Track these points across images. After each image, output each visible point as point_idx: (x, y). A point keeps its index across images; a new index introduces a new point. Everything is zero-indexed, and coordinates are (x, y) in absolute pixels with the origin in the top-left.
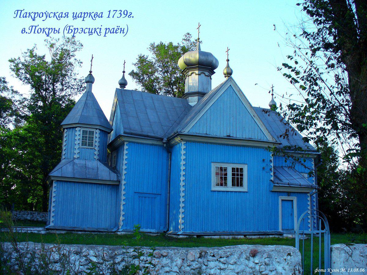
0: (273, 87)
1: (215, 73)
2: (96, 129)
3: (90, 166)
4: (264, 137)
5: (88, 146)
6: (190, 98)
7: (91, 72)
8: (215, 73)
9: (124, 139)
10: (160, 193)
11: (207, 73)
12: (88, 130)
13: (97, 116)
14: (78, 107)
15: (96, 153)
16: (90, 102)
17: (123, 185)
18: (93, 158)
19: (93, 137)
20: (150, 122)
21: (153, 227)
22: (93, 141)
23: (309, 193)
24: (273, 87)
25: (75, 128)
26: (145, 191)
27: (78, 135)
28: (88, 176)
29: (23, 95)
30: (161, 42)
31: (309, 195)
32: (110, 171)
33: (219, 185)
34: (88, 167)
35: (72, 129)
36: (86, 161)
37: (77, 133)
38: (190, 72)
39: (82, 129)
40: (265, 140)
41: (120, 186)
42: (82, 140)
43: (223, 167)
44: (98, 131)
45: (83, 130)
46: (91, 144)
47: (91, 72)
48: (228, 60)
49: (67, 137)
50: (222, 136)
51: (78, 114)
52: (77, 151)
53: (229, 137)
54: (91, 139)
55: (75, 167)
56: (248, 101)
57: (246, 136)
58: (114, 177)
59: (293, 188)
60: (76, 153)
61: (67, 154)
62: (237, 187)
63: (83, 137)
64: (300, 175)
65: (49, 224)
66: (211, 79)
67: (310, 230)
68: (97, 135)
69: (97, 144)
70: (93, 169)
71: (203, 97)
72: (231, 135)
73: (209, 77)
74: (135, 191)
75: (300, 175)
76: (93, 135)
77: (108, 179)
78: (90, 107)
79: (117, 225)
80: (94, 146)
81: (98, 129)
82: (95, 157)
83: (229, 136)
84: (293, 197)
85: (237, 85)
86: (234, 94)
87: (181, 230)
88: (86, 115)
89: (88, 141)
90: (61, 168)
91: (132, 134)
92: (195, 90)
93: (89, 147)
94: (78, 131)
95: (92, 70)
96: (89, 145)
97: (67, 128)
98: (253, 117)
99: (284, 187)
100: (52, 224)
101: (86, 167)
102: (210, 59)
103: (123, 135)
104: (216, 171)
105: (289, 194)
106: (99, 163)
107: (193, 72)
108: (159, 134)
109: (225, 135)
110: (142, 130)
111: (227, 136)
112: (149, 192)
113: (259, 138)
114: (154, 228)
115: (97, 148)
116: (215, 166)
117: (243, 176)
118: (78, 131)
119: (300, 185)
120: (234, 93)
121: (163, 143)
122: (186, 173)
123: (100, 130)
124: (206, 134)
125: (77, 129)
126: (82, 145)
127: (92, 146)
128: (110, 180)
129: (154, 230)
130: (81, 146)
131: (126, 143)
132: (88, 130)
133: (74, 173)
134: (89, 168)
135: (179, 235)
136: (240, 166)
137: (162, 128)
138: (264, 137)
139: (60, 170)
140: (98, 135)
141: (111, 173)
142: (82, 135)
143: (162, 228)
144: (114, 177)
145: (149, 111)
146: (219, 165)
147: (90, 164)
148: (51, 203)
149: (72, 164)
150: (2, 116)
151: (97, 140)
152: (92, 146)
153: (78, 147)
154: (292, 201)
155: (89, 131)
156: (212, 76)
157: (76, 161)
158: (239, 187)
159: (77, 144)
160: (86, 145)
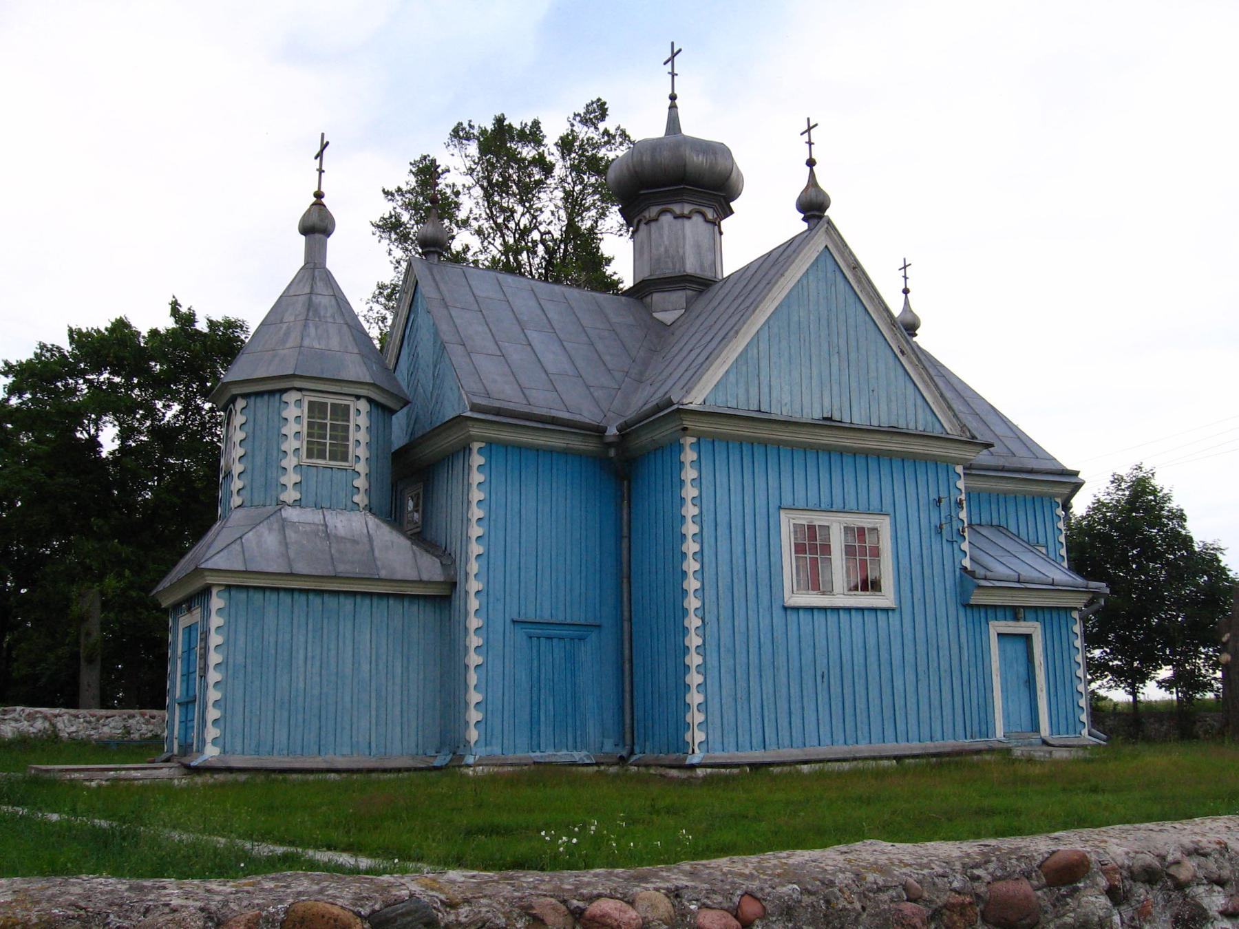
0: (905, 267)
1: (732, 212)
2: (358, 397)
3: (342, 531)
4: (933, 426)
5: (330, 459)
6: (656, 296)
7: (319, 195)
8: (732, 212)
9: (475, 431)
10: (598, 622)
11: (710, 214)
12: (330, 400)
13: (356, 351)
14: (282, 318)
15: (360, 483)
16: (324, 301)
17: (472, 595)
18: (349, 503)
19: (347, 428)
20: (547, 374)
21: (579, 744)
22: (348, 440)
23: (1075, 609)
24: (905, 267)
25: (277, 396)
26: (547, 617)
27: (291, 418)
28: (342, 568)
29: (446, 136)
30: (503, 115)
31: (1075, 615)
32: (415, 548)
33: (856, 588)
34: (336, 536)
35: (266, 397)
36: (324, 514)
37: (291, 412)
38: (654, 211)
39: (308, 398)
40: (937, 432)
41: (457, 602)
42: (309, 435)
43: (817, 523)
44: (363, 405)
45: (310, 403)
46: (341, 454)
47: (319, 195)
48: (811, 163)
49: (249, 427)
50: (806, 418)
51: (290, 344)
52: (291, 478)
53: (828, 423)
54: (341, 434)
55: (291, 535)
56: (883, 302)
57: (881, 418)
58: (431, 569)
59: (1034, 593)
60: (290, 486)
61: (248, 488)
62: (863, 593)
63: (310, 425)
64: (1034, 551)
65: (201, 751)
66: (721, 233)
67: (1085, 732)
68: (360, 419)
69: (362, 452)
70: (355, 542)
71: (701, 292)
72: (836, 417)
73: (716, 227)
74: (516, 618)
75: (1034, 551)
76: (348, 421)
77: (413, 575)
78: (330, 320)
79: (451, 740)
80: (350, 458)
81: (364, 397)
82: (357, 499)
83: (830, 419)
84: (1030, 624)
85: (846, 245)
86: (839, 278)
87: (697, 750)
88: (318, 347)
89: (328, 441)
90: (239, 541)
91: (498, 412)
92: (674, 269)
93: (332, 463)
94: (292, 405)
95: (322, 190)
96: (333, 457)
97: (245, 396)
98: (899, 355)
99: (1006, 592)
100: (211, 752)
101: (328, 536)
102: (722, 164)
103: (469, 414)
104: (795, 538)
105: (1015, 613)
106: (372, 521)
107: (664, 207)
108: (588, 414)
109: (817, 415)
110: (527, 400)
111: (825, 419)
112: (561, 619)
113: (921, 428)
114: (585, 746)
115: (361, 467)
116: (792, 522)
117: (830, 555)
118: (292, 405)
119: (1019, 582)
120: (838, 273)
121: (607, 444)
122: (702, 546)
123: (370, 400)
124: (760, 411)
125: (292, 397)
126: (310, 454)
127: (345, 459)
128: (421, 581)
129: (584, 753)
130: (305, 460)
131: (476, 446)
132: (330, 400)
133: (289, 558)
134: (340, 539)
135: (693, 767)
136: (869, 523)
137: (591, 393)
138: (933, 426)
139: (237, 547)
140: (363, 421)
141: (418, 553)
142: (309, 417)
143: (609, 746)
144: (431, 569)
145: (533, 335)
146: (804, 519)
147: (339, 525)
148: (711, 758)
149: (276, 526)
150: (529, 201)
151: (363, 436)
152: (345, 459)
153: (294, 461)
154: (1028, 638)
155: (332, 404)
156: (725, 224)
157: (291, 514)
158: (868, 593)
159: (290, 453)
160: (322, 455)
